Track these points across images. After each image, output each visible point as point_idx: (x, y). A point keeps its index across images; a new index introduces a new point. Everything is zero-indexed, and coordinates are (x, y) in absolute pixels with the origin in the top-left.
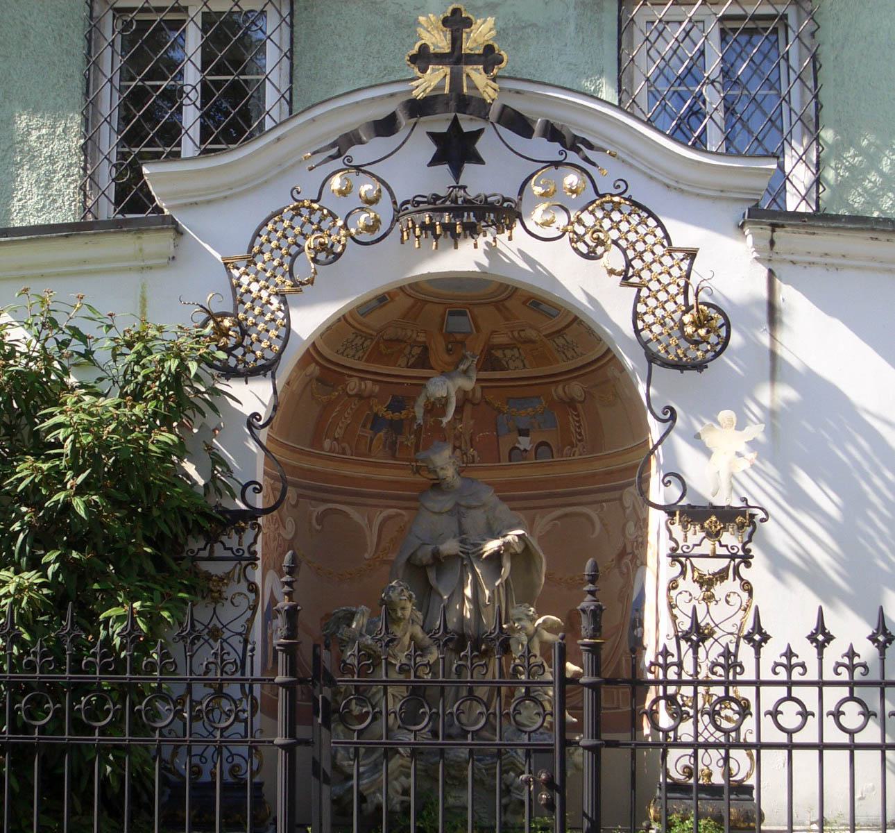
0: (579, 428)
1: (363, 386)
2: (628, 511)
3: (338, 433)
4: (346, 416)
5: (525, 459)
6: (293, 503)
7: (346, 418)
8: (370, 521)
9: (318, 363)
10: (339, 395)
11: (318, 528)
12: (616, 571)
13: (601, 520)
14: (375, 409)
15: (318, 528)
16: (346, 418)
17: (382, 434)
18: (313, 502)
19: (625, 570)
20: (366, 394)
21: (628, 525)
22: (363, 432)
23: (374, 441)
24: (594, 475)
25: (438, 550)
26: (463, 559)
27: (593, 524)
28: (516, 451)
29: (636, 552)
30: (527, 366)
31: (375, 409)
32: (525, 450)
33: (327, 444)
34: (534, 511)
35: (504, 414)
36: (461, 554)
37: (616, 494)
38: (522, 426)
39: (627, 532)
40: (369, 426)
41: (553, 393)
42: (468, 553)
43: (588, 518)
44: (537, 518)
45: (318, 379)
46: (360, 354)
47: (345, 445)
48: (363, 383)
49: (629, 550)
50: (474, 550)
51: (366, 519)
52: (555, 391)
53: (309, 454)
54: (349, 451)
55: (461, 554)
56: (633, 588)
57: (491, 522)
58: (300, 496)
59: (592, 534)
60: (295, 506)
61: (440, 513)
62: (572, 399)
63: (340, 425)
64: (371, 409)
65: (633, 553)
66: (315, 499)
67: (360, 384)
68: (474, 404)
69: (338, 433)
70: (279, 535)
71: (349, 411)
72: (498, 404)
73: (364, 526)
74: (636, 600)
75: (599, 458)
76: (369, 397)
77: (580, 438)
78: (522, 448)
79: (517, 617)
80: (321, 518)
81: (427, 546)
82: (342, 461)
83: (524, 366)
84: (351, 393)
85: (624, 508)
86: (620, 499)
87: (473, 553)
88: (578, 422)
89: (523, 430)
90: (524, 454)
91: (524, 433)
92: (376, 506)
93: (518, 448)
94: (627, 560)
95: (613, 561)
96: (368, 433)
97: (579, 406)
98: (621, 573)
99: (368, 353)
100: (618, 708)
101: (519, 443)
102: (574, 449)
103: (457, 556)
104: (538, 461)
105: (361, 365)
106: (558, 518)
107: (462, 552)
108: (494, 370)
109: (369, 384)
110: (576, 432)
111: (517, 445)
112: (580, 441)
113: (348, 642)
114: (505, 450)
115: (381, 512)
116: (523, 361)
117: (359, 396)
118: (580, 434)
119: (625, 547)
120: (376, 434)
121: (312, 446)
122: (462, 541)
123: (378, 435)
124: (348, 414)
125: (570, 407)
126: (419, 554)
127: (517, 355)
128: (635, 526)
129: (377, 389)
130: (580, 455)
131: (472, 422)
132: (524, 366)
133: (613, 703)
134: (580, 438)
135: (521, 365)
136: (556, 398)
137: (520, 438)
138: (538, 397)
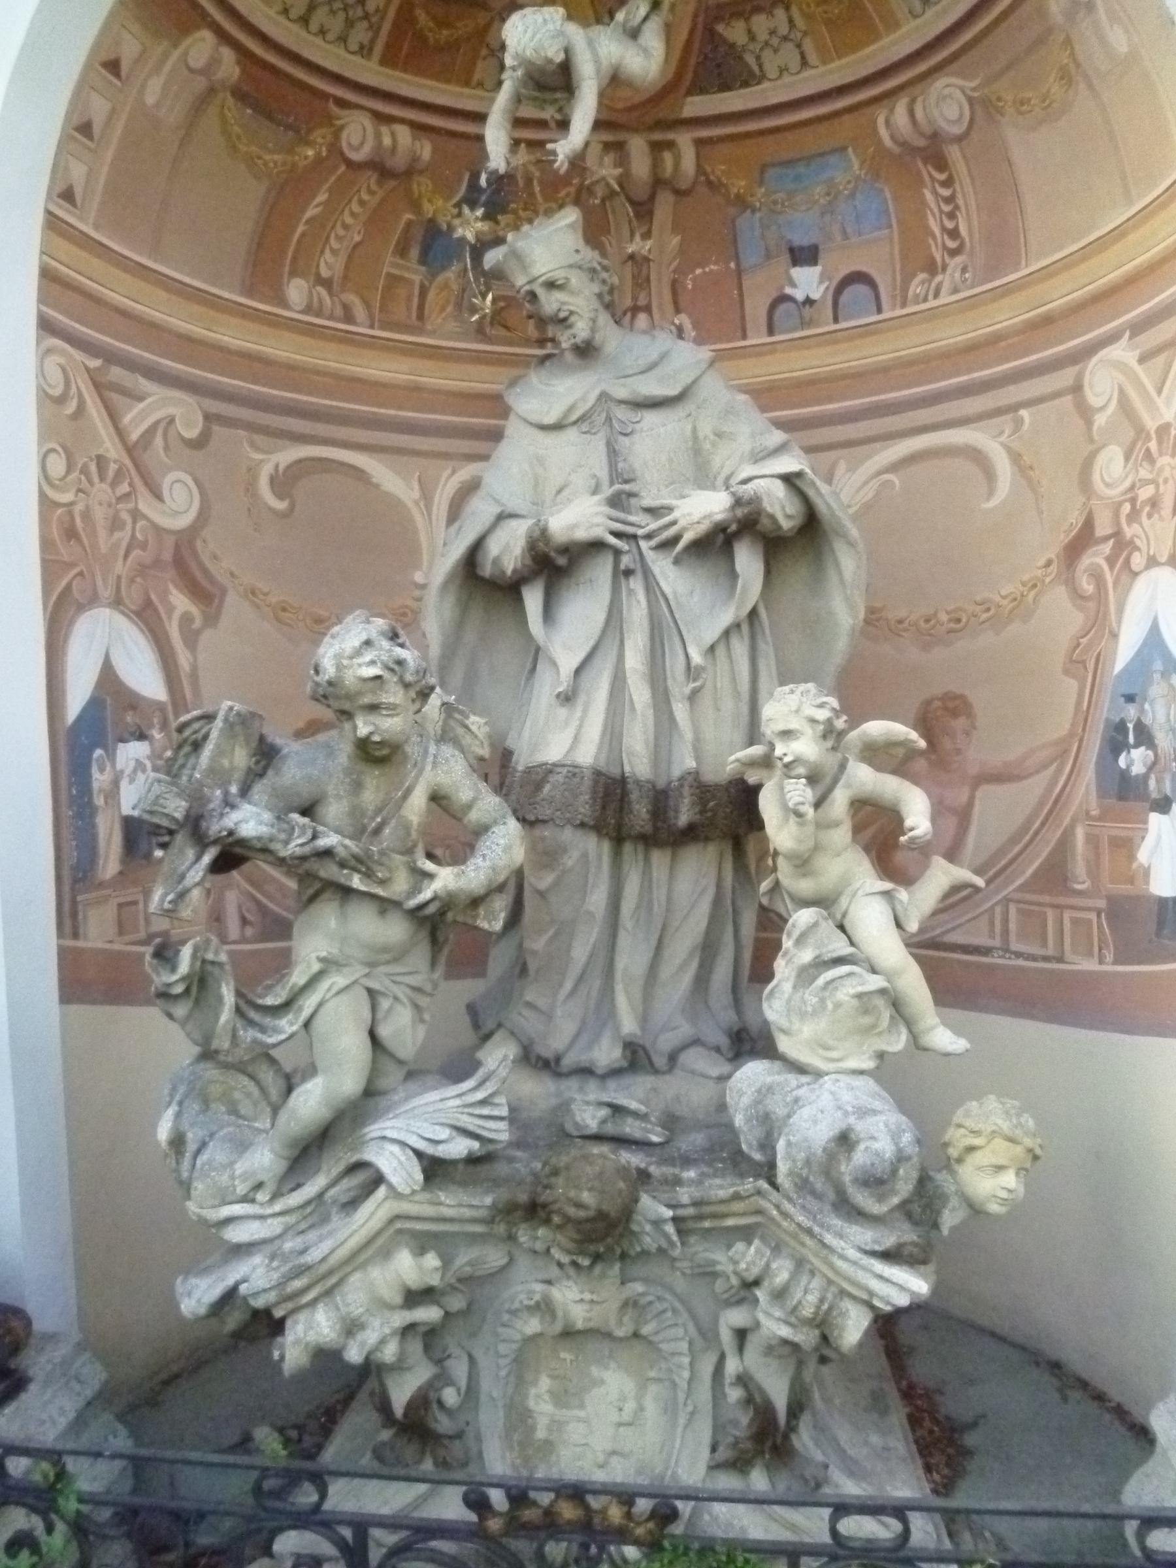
0: (952, 216)
1: (387, 141)
2: (1100, 420)
3: (330, 264)
4: (349, 220)
5: (804, 324)
6: (192, 433)
7: (346, 227)
8: (427, 496)
9: (223, 36)
10: (318, 161)
11: (281, 505)
12: (1060, 593)
13: (1016, 458)
14: (428, 209)
15: (281, 505)
16: (346, 227)
17: (450, 274)
18: (258, 438)
19: (1088, 588)
20: (399, 162)
21: (1101, 459)
22: (397, 266)
23: (431, 295)
24: (994, 340)
25: (544, 531)
26: (617, 553)
27: (990, 475)
28: (783, 308)
29: (1129, 531)
30: (812, 58)
31: (428, 209)
32: (809, 302)
33: (297, 291)
34: (833, 455)
35: (753, 211)
36: (612, 540)
37: (1064, 378)
38: (800, 239)
39: (1096, 477)
40: (415, 253)
41: (883, 132)
42: (634, 537)
43: (977, 456)
44: (842, 467)
45: (239, 94)
46: (360, 34)
47: (352, 298)
48: (384, 130)
49: (1103, 528)
50: (654, 525)
51: (416, 486)
52: (887, 123)
53: (245, 313)
54: (360, 311)
55: (612, 540)
56: (1115, 636)
57: (707, 446)
58: (208, 417)
59: (991, 493)
60: (199, 444)
61: (558, 427)
62: (935, 137)
63: (334, 243)
64: (416, 206)
65: (1117, 534)
66: (267, 431)
67: (378, 136)
68: (677, 192)
69: (330, 264)
70: (136, 514)
71: (355, 207)
72: (738, 185)
73: (410, 504)
74: (1126, 670)
75: (1007, 291)
76: (409, 173)
77: (952, 244)
78: (799, 295)
79: (781, 727)
80: (283, 483)
81: (513, 523)
82: (348, 339)
83: (804, 63)
84: (356, 157)
85: (1086, 412)
86: (1077, 389)
87: (649, 537)
88: (949, 200)
89: (802, 249)
90: (807, 311)
91: (804, 255)
92: (446, 456)
93: (789, 299)
94: (1096, 557)
95: (1049, 564)
96: (416, 275)
97: (954, 153)
98: (1077, 596)
99: (386, 27)
100: (1060, 960)
101: (793, 285)
102: (939, 278)
103: (596, 546)
104: (838, 327)
105: (371, 73)
106: (894, 467)
107: (617, 535)
108: (725, 87)
109: (404, 134)
110: (944, 229)
111: (788, 290)
112: (954, 253)
113: (171, 833)
114: (756, 307)
115: (454, 472)
116: (799, 46)
117: (379, 167)
118: (954, 234)
119: (1088, 525)
120: (433, 276)
121: (250, 292)
122: (615, 501)
123: (440, 278)
124: (353, 214)
125: (926, 161)
126: (494, 547)
127: (784, 29)
128: (1127, 459)
129: (426, 151)
130: (955, 291)
131: (676, 240)
132: (804, 63)
133: (1044, 943)
134: (952, 244)
135: (795, 62)
136: (888, 142)
137: (798, 273)
138: (844, 149)
